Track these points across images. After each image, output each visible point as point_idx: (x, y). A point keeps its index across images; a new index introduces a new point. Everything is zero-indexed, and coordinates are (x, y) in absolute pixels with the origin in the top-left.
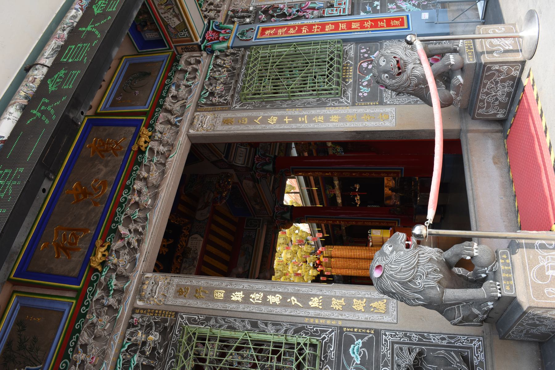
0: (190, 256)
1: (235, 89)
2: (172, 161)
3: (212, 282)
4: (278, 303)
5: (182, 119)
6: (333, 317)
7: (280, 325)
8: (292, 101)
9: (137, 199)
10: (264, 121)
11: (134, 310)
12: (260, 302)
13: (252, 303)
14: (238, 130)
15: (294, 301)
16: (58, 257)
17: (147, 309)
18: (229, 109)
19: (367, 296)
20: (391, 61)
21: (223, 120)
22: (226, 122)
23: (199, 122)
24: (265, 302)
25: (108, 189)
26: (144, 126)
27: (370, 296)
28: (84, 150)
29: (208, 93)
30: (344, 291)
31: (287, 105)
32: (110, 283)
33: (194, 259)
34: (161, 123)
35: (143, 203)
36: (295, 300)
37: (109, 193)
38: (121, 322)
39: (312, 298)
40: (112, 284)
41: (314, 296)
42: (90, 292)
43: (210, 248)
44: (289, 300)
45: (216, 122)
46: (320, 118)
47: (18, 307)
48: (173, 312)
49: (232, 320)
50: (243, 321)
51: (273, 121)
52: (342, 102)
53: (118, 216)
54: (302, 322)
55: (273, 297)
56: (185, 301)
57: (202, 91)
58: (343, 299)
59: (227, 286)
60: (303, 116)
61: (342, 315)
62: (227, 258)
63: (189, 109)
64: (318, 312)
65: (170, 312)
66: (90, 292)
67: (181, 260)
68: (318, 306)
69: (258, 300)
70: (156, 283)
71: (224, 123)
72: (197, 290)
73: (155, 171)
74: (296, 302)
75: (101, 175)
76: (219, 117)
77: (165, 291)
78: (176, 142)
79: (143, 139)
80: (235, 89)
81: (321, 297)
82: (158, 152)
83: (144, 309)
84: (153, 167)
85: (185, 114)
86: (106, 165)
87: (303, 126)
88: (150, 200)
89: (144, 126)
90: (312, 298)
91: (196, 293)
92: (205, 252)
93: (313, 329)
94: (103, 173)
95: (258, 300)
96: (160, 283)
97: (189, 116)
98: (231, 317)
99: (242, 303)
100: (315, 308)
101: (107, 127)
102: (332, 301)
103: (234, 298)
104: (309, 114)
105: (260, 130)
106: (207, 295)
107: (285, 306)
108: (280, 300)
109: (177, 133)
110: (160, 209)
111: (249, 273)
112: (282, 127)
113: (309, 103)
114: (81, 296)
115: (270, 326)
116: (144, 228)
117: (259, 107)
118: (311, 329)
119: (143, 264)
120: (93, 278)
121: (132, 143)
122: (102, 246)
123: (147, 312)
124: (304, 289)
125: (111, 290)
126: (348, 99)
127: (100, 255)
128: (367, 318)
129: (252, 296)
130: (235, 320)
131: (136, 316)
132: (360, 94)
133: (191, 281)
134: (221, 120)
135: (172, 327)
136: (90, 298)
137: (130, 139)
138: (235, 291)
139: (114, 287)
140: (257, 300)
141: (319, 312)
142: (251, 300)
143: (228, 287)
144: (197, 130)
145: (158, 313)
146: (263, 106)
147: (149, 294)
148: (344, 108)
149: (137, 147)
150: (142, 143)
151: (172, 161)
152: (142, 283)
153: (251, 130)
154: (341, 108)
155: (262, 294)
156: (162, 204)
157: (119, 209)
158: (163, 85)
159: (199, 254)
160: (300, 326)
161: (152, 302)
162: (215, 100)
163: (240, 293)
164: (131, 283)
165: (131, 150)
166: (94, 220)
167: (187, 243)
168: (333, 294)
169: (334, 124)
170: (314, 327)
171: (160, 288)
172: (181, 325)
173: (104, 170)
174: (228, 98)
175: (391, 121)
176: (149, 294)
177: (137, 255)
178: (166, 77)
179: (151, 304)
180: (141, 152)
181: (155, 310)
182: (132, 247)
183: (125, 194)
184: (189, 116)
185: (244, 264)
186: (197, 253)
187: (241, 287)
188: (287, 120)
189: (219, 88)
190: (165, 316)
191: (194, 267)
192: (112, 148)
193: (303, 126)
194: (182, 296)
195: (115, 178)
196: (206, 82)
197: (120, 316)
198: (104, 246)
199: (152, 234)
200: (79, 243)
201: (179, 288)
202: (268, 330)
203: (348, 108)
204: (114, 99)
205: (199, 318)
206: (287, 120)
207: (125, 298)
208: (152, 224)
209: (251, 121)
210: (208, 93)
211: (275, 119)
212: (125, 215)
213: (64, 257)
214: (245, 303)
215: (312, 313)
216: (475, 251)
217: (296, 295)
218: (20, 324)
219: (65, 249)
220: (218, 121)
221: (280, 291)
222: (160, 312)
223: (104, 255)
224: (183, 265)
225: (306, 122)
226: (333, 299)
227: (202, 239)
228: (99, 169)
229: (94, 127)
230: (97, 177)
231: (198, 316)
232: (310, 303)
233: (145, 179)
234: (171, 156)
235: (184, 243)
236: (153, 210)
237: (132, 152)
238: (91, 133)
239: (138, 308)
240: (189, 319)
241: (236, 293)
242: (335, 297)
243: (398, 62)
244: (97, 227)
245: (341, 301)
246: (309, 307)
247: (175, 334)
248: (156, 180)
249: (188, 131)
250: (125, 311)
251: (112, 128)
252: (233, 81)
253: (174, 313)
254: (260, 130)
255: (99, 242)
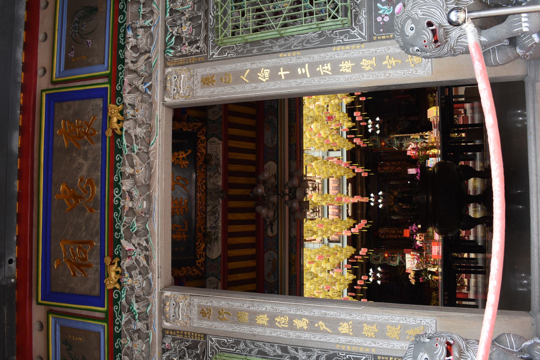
0: (213, 163)
1: (206, 25)
2: (155, 148)
3: (233, 303)
4: (305, 328)
5: (151, 85)
6: (366, 345)
7: (312, 351)
8: (286, 40)
9: (130, 205)
10: (254, 77)
11: (164, 332)
12: (287, 326)
13: (278, 328)
14: (223, 95)
15: (322, 326)
16: (74, 275)
17: (176, 331)
18: (206, 60)
19: (401, 322)
20: (424, 34)
21: (202, 78)
22: (207, 81)
23: (173, 87)
24: (292, 327)
25: (97, 190)
26: (110, 103)
27: (405, 322)
28: (55, 138)
29: (174, 38)
30: (375, 316)
31: (280, 46)
32: (132, 308)
33: (217, 165)
34: (128, 93)
35: (138, 209)
36: (323, 324)
37: (99, 195)
38: (155, 344)
39: (341, 324)
40: (135, 309)
41: (344, 320)
42: (117, 310)
43: (232, 144)
44: (316, 325)
45: (193, 82)
46: (326, 68)
47: (58, 327)
48: (202, 334)
49: (261, 344)
50: (273, 346)
51: (264, 78)
52: (354, 37)
53: (118, 223)
54: (333, 348)
55: (299, 321)
56: (210, 323)
57: (165, 37)
58: (375, 325)
59: (249, 307)
60: (302, 66)
61: (375, 343)
62: (252, 157)
63: (157, 65)
64: (349, 339)
65: (198, 334)
66: (117, 310)
67: (205, 169)
68: (348, 332)
69: (284, 324)
70: (177, 305)
71: (204, 83)
72: (219, 312)
73: (140, 165)
74: (324, 327)
75: (84, 172)
76: (197, 75)
77: (187, 310)
78: (153, 121)
79: (115, 120)
80: (206, 25)
81: (351, 322)
82: (135, 136)
83: (173, 331)
84: (137, 160)
85: (154, 76)
86: (86, 158)
87: (304, 82)
88: (145, 202)
89: (110, 103)
90: (341, 324)
91: (220, 315)
92: (227, 149)
93: (346, 356)
94: (85, 168)
95: (284, 324)
96: (181, 304)
97: (159, 76)
98: (259, 341)
99: (268, 327)
100: (346, 335)
101: (71, 103)
102: (363, 327)
103: (259, 322)
104: (311, 60)
105: (251, 92)
106: (231, 317)
107: (313, 331)
108: (308, 325)
109: (151, 104)
110: (158, 213)
111: (278, 147)
112: (277, 87)
113: (308, 42)
114: (110, 318)
115: (300, 352)
116: (147, 241)
117: (242, 52)
118: (343, 356)
119: (158, 281)
120: (116, 296)
121: (104, 128)
122: (112, 264)
123: (176, 333)
124: (332, 313)
125: (136, 314)
126: (361, 29)
127: (113, 274)
128: (402, 347)
129: (277, 319)
130: (264, 345)
131: (168, 341)
132: (379, 19)
133: (211, 302)
134: (200, 79)
135: (204, 353)
136: (119, 317)
137: (101, 117)
138: (259, 313)
139: (137, 311)
140: (283, 324)
141: (350, 339)
142: (277, 324)
143: (251, 308)
144: (174, 98)
145: (187, 335)
146: (248, 51)
147: (173, 316)
148: (358, 46)
149: (111, 131)
150: (116, 126)
151: (155, 148)
152: (163, 303)
153: (239, 93)
154: (353, 46)
155: (287, 318)
156: (158, 206)
157: (115, 214)
158: (117, 27)
159: (221, 159)
160: (331, 352)
161: (179, 324)
162: (186, 49)
163: (264, 316)
164: (152, 305)
165: (106, 137)
166: (95, 230)
167: (206, 148)
168: (363, 318)
169: (347, 76)
170: (347, 354)
171: (182, 310)
172: (212, 348)
173: (86, 165)
174: (201, 44)
175: (425, 67)
176: (173, 316)
177: (150, 276)
178: (118, 12)
179: (178, 325)
180: (116, 136)
181: (184, 332)
182: (141, 265)
183: (117, 194)
184: (159, 76)
185: (272, 138)
186: (219, 159)
187: (264, 309)
188: (282, 73)
189: (186, 29)
190: (194, 338)
191: (220, 174)
192: (85, 132)
193: (304, 82)
194: (206, 318)
195: (100, 174)
196: (168, 19)
197: (153, 341)
198: (114, 264)
199: (158, 245)
200: (90, 259)
201: (200, 309)
202: (299, 355)
203: (363, 46)
204: (66, 55)
205: (228, 341)
206: (282, 73)
207: (151, 322)
208: (154, 234)
209: (237, 77)
210: (174, 38)
211: (267, 73)
212: (123, 226)
213: (80, 275)
214: (271, 327)
215: (343, 339)
216: (524, 25)
217: (324, 319)
218: (65, 342)
219: (79, 266)
220: (196, 82)
221: (306, 314)
222: (189, 334)
223: (117, 273)
224: (208, 174)
225: (309, 76)
226: (365, 325)
227: (221, 142)
228: (79, 164)
229: (57, 105)
230: (80, 175)
231: (227, 339)
232: (340, 329)
233: (132, 175)
234: (152, 142)
235: (204, 150)
236: (152, 219)
237: (108, 139)
238: (56, 113)
239: (167, 329)
240: (218, 342)
241: (260, 316)
242: (366, 322)
243: (434, 32)
244: (101, 237)
245: (373, 328)
246: (339, 334)
247: (209, 357)
248: (143, 177)
249: (163, 100)
250: (155, 334)
251: (76, 105)
252: (201, 14)
253: (202, 336)
254: (251, 92)
255: (108, 260)
